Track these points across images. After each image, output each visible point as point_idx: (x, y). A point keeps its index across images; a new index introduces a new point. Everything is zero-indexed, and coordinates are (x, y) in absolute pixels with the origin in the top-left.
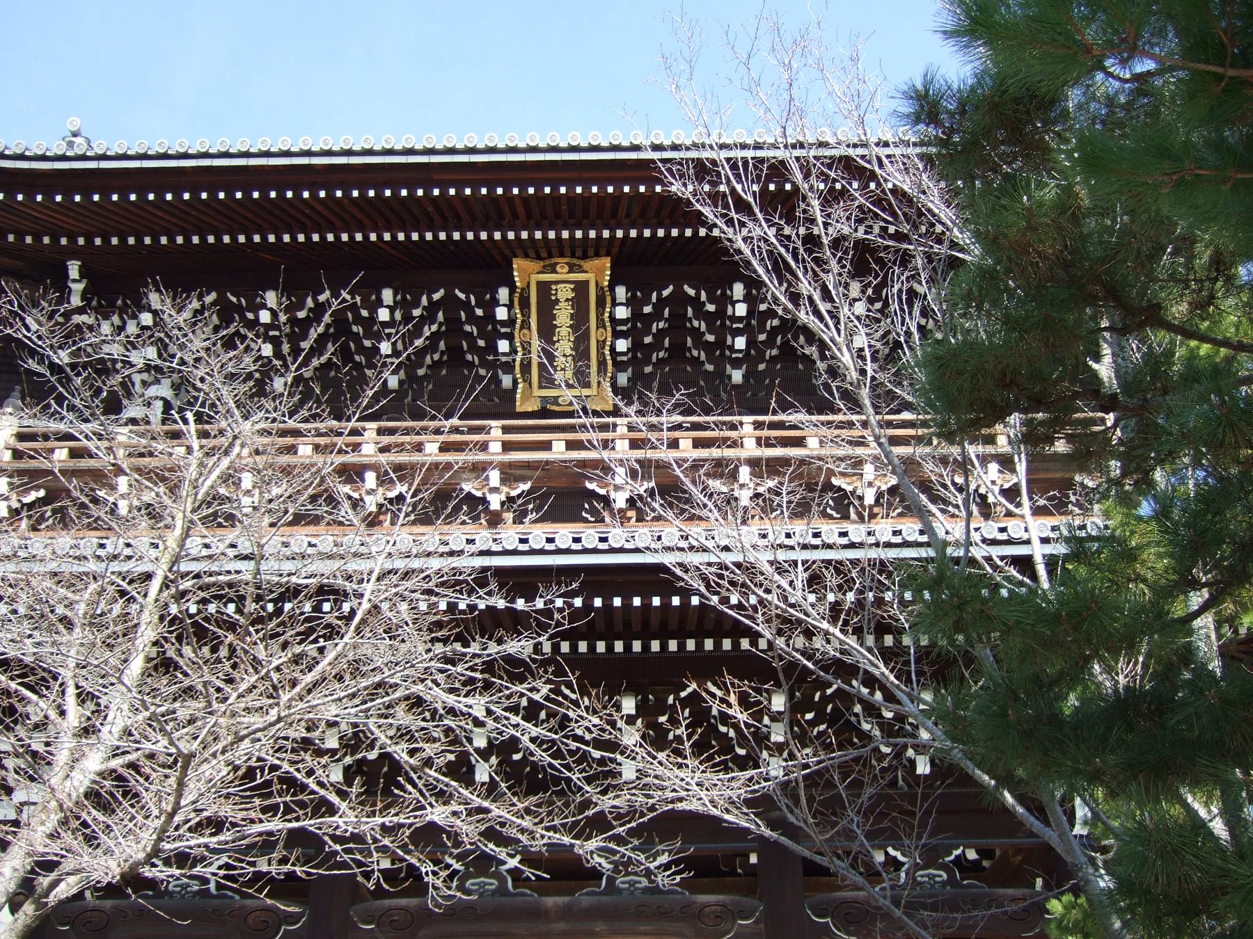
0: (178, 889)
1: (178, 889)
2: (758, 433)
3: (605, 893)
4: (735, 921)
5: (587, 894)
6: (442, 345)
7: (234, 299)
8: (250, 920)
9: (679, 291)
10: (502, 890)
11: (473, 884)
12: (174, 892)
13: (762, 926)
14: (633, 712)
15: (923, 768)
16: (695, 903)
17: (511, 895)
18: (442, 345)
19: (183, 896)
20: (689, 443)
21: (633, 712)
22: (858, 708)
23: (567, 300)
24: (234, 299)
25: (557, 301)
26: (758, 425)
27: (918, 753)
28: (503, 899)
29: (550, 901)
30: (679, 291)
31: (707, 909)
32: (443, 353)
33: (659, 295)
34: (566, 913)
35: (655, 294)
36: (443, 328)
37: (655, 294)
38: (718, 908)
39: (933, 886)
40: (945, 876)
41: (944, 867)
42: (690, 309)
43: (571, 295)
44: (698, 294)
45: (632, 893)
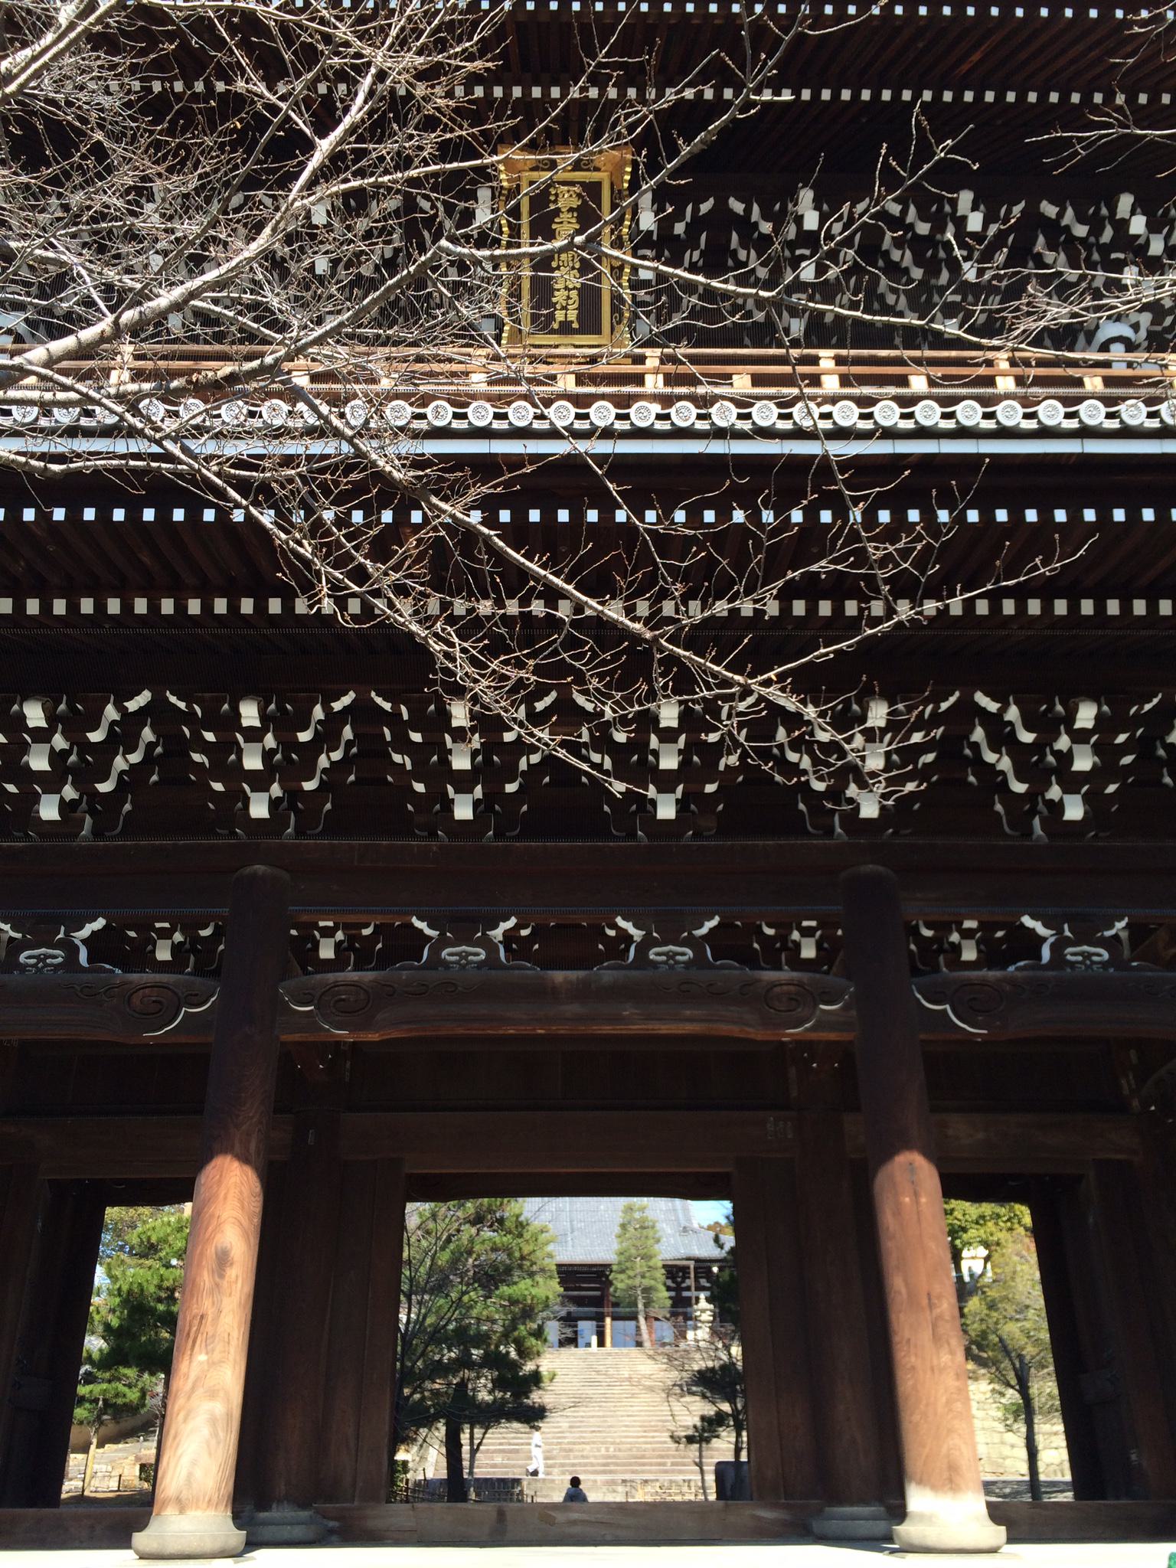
0: (33, 961)
1: (33, 961)
2: (844, 369)
3: (634, 966)
4: (816, 1005)
5: (608, 968)
6: (348, 733)
7: (182, 705)
8: (136, 1000)
9: (721, 206)
10: (492, 962)
11: (450, 954)
12: (27, 965)
13: (854, 1013)
14: (675, 724)
15: (1074, 810)
16: (759, 981)
17: (503, 967)
18: (348, 733)
19: (39, 970)
20: (747, 379)
21: (675, 724)
22: (978, 735)
23: (571, 210)
24: (182, 705)
25: (557, 212)
26: (840, 361)
27: (1066, 790)
28: (493, 972)
29: (559, 976)
30: (721, 206)
31: (777, 990)
32: (349, 744)
33: (696, 210)
34: (581, 992)
35: (689, 208)
36: (354, 750)
37: (689, 208)
38: (792, 988)
39: (1088, 967)
40: (1106, 955)
41: (1104, 943)
42: (735, 236)
43: (576, 203)
44: (748, 210)
45: (671, 967)
